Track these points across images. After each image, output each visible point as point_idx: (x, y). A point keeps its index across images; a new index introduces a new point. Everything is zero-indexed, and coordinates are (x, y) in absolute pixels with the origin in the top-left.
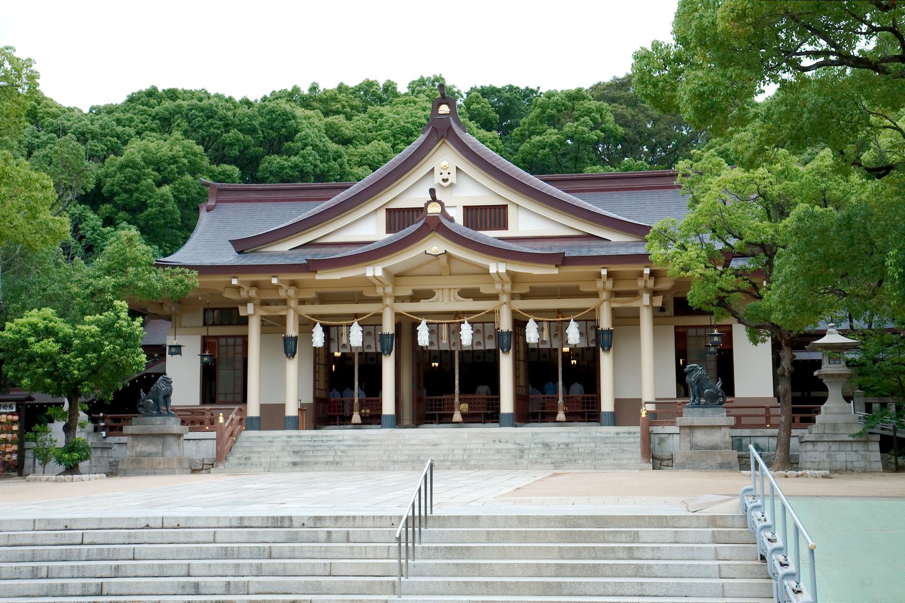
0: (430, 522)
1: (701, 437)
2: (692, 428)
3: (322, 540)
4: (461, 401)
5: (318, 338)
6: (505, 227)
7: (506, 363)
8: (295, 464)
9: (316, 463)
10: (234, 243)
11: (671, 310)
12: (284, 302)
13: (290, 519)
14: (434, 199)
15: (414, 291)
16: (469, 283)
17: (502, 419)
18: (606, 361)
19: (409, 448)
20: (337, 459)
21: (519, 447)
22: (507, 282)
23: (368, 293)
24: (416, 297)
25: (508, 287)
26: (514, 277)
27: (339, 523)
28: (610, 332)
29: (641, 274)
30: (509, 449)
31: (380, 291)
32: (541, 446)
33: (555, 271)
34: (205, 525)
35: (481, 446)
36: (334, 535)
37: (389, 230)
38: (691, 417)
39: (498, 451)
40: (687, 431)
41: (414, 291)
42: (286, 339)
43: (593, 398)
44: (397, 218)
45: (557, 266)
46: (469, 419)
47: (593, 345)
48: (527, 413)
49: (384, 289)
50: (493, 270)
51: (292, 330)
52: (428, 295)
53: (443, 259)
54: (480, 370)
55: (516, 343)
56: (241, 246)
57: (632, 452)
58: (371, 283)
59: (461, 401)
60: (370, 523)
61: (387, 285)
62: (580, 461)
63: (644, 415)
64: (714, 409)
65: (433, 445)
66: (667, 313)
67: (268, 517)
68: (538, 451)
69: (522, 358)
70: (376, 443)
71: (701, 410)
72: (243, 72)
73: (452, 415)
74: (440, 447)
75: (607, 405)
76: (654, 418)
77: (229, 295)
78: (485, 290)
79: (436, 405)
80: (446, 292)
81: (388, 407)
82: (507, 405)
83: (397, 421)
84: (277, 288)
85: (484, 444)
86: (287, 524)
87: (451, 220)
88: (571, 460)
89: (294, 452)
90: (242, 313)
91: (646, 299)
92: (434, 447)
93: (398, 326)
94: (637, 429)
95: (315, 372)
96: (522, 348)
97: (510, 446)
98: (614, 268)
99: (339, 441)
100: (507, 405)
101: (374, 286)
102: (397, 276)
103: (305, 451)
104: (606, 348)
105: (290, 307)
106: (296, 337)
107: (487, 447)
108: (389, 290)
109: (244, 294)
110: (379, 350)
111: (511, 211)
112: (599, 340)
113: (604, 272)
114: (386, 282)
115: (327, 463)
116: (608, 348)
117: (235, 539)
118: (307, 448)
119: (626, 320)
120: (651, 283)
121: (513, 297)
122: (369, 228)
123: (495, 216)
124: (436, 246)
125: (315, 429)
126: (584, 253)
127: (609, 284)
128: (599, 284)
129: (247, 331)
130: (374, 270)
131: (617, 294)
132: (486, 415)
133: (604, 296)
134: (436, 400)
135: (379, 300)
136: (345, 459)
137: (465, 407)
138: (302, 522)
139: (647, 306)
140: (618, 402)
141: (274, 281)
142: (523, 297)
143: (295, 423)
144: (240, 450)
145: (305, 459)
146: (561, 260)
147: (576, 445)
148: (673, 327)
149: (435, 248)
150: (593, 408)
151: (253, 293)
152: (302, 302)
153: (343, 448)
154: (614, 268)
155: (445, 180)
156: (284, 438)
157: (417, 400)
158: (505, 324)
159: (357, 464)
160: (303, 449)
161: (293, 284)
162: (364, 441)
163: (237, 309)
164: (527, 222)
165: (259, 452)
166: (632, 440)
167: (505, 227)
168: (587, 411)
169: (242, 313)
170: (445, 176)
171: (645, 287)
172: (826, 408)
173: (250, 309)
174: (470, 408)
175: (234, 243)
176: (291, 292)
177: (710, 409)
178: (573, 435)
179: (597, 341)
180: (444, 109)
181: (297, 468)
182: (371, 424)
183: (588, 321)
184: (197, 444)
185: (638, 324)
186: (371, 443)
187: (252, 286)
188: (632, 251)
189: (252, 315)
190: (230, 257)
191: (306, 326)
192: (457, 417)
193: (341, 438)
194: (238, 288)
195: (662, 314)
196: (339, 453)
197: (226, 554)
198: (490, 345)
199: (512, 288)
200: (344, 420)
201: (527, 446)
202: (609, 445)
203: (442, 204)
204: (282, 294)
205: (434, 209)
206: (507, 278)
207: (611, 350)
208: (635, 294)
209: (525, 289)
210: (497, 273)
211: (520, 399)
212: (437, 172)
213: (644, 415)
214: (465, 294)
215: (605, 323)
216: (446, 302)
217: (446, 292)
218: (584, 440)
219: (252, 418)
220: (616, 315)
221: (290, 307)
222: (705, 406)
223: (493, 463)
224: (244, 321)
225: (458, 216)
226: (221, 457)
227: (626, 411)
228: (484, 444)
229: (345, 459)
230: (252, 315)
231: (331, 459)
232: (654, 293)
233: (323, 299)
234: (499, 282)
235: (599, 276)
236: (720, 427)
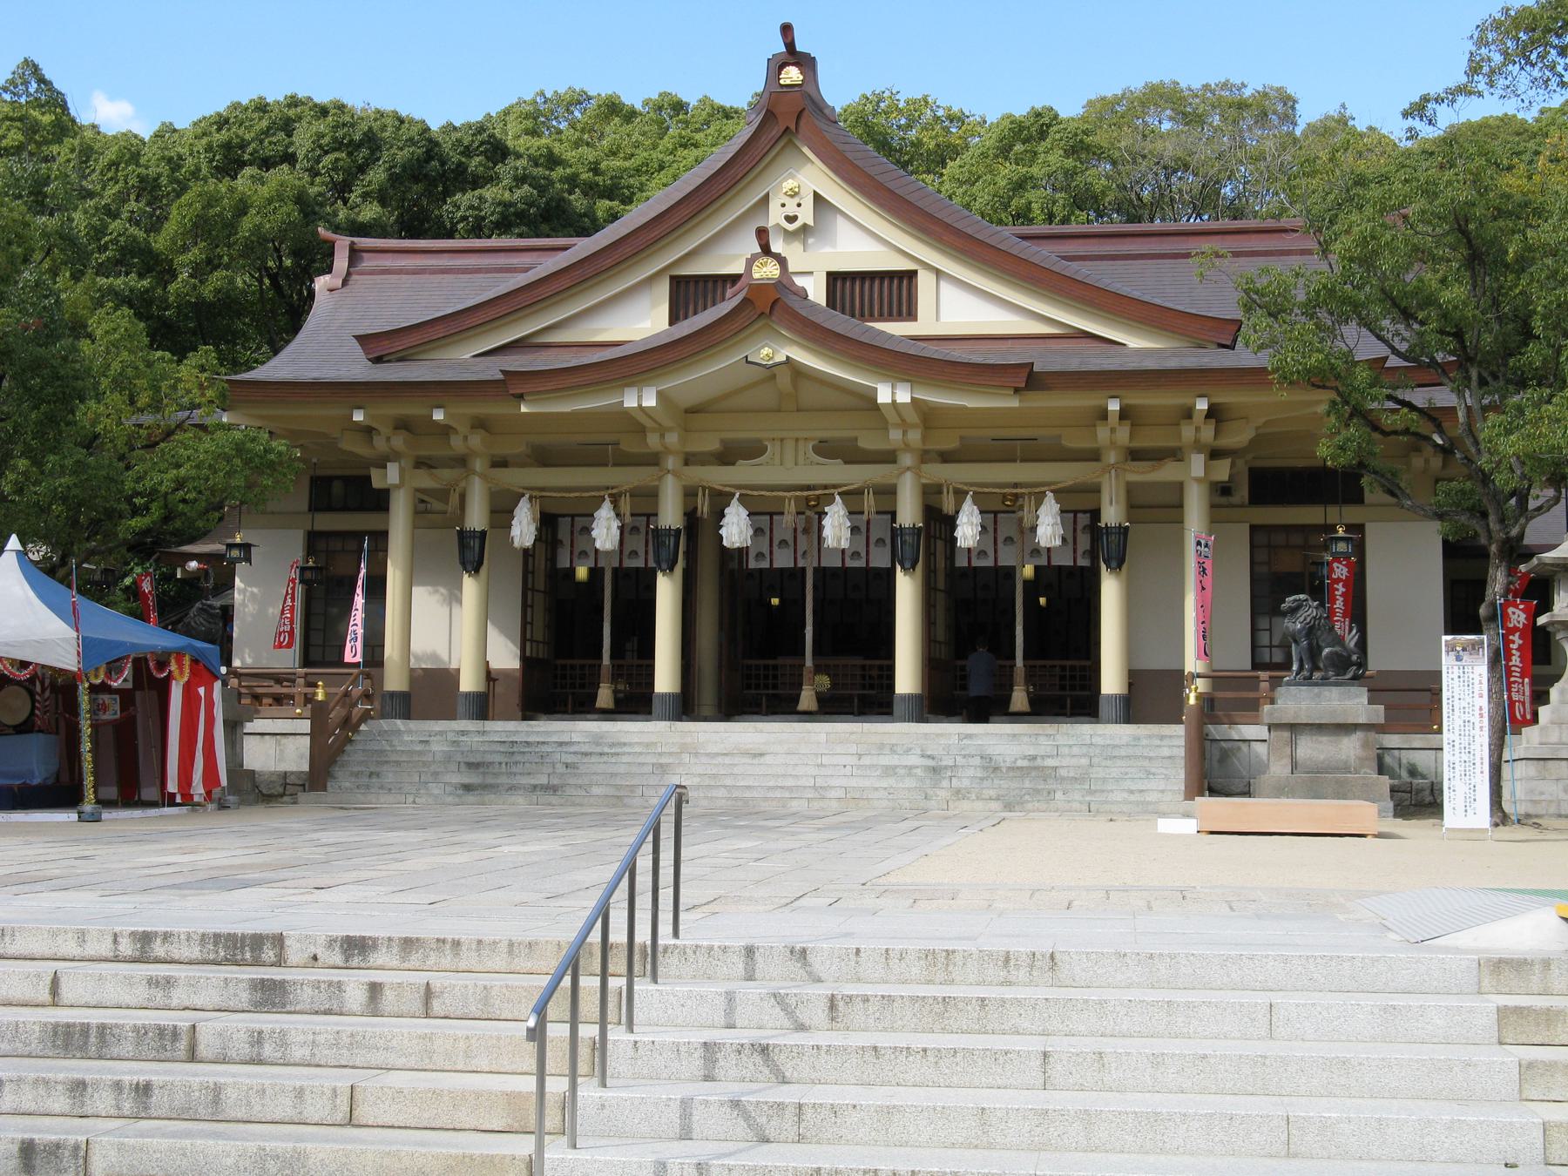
0: (667, 964)
1: (1311, 749)
2: (1295, 728)
3: (356, 1007)
4: (818, 669)
5: (523, 530)
6: (911, 315)
7: (907, 592)
8: (468, 788)
9: (512, 788)
10: (358, 338)
11: (1242, 493)
12: (462, 461)
13: (279, 940)
14: (766, 250)
15: (722, 441)
16: (837, 430)
17: (898, 708)
18: (1111, 591)
19: (704, 760)
20: (555, 781)
21: (931, 763)
22: (913, 426)
23: (629, 446)
24: (726, 456)
25: (915, 436)
26: (927, 416)
27: (415, 959)
28: (1123, 532)
29: (1188, 413)
30: (911, 768)
31: (653, 441)
32: (977, 761)
33: (1014, 403)
34: (48, 953)
35: (853, 760)
36: (389, 995)
37: (673, 320)
38: (1296, 701)
39: (889, 771)
40: (1286, 734)
41: (722, 441)
42: (463, 536)
43: (1083, 668)
44: (688, 293)
45: (1017, 390)
46: (832, 707)
47: (1083, 562)
48: (956, 695)
49: (662, 436)
50: (884, 395)
51: (476, 518)
52: (753, 451)
53: (784, 380)
54: (857, 613)
55: (930, 554)
56: (377, 345)
57: (1167, 778)
58: (634, 423)
59: (818, 669)
60: (499, 962)
61: (670, 429)
62: (1059, 795)
63: (1192, 701)
64: (1342, 689)
65: (755, 756)
66: (1235, 499)
67: (217, 936)
68: (971, 772)
69: (941, 585)
70: (637, 749)
71: (1316, 689)
72: (445, 95)
73: (796, 699)
74: (768, 759)
75: (1111, 681)
76: (1210, 709)
77: (353, 445)
78: (868, 442)
79: (766, 677)
80: (790, 445)
81: (665, 678)
82: (907, 678)
83: (685, 707)
84: (445, 430)
85: (860, 756)
86: (269, 954)
87: (802, 294)
88: (1038, 791)
89: (470, 765)
90: (377, 483)
91: (1197, 464)
92: (756, 761)
93: (691, 516)
94: (1178, 731)
95: (525, 606)
96: (941, 564)
97: (914, 760)
98: (1139, 399)
99: (561, 744)
100: (907, 678)
101: (641, 430)
102: (691, 411)
103: (492, 763)
104: (1114, 564)
105: (474, 472)
106: (483, 534)
107: (866, 761)
108: (672, 439)
109: (380, 444)
110: (652, 564)
111: (925, 281)
112: (1101, 545)
113: (1114, 406)
114: (667, 423)
115: (535, 787)
116: (1117, 562)
117: (112, 993)
118: (497, 758)
119: (1160, 508)
120: (1208, 433)
121: (925, 457)
122: (643, 320)
123: (892, 291)
124: (775, 350)
125: (525, 718)
126: (1074, 365)
127: (1123, 435)
128: (1103, 434)
129: (387, 523)
130: (640, 398)
131: (1135, 455)
132: (862, 698)
133: (1112, 457)
134: (766, 667)
135: (653, 460)
136: (572, 781)
137: (824, 681)
138: (312, 950)
139: (1198, 480)
140: (1135, 677)
141: (438, 415)
142: (946, 457)
143: (481, 707)
144: (359, 757)
145: (490, 780)
146: (1030, 380)
147: (1050, 762)
148: (1247, 526)
149: (766, 351)
150: (1083, 688)
151: (398, 442)
152: (500, 463)
153: (570, 759)
154: (1139, 399)
155: (791, 219)
156: (451, 737)
157: (728, 661)
158: (909, 514)
159: (596, 790)
160: (489, 758)
161: (480, 424)
162: (612, 745)
163: (369, 478)
164: (961, 306)
165: (398, 763)
166: (1166, 752)
167: (911, 315)
168: (1069, 695)
169: (377, 483)
170: (791, 209)
171: (1197, 441)
172: (1562, 692)
173: (392, 474)
174: (834, 685)
175: (358, 338)
176: (476, 441)
177: (1334, 689)
178: (1042, 740)
179: (1093, 554)
180: (792, 75)
181: (470, 798)
182: (636, 713)
183: (1081, 512)
184: (278, 743)
185: (1180, 521)
186: (626, 749)
187: (396, 428)
188: (1173, 364)
189: (397, 487)
190: (357, 368)
191: (502, 513)
192: (807, 700)
193: (567, 739)
194: (368, 431)
195: (1224, 500)
196: (560, 769)
197: (69, 1040)
198: (880, 559)
199: (924, 438)
200: (583, 707)
201: (948, 762)
202: (1119, 763)
203: (781, 261)
204: (457, 444)
205: (767, 271)
206: (913, 418)
207: (1125, 566)
208: (1174, 454)
209: (950, 443)
210: (640, 406)
211: (932, 665)
212: (774, 205)
213: (1192, 701)
214: (827, 449)
215: (1112, 515)
216: (787, 467)
217: (790, 445)
218: (1066, 750)
219: (392, 694)
220: (1136, 504)
221: (474, 472)
222: (1325, 681)
223: (876, 795)
224: (380, 502)
225: (816, 291)
226: (319, 776)
227: (1151, 697)
228: (860, 756)
229: (572, 781)
230: (397, 487)
231: (544, 780)
232: (1215, 454)
233: (544, 457)
234: (897, 426)
235: (1104, 415)
236: (1355, 727)
